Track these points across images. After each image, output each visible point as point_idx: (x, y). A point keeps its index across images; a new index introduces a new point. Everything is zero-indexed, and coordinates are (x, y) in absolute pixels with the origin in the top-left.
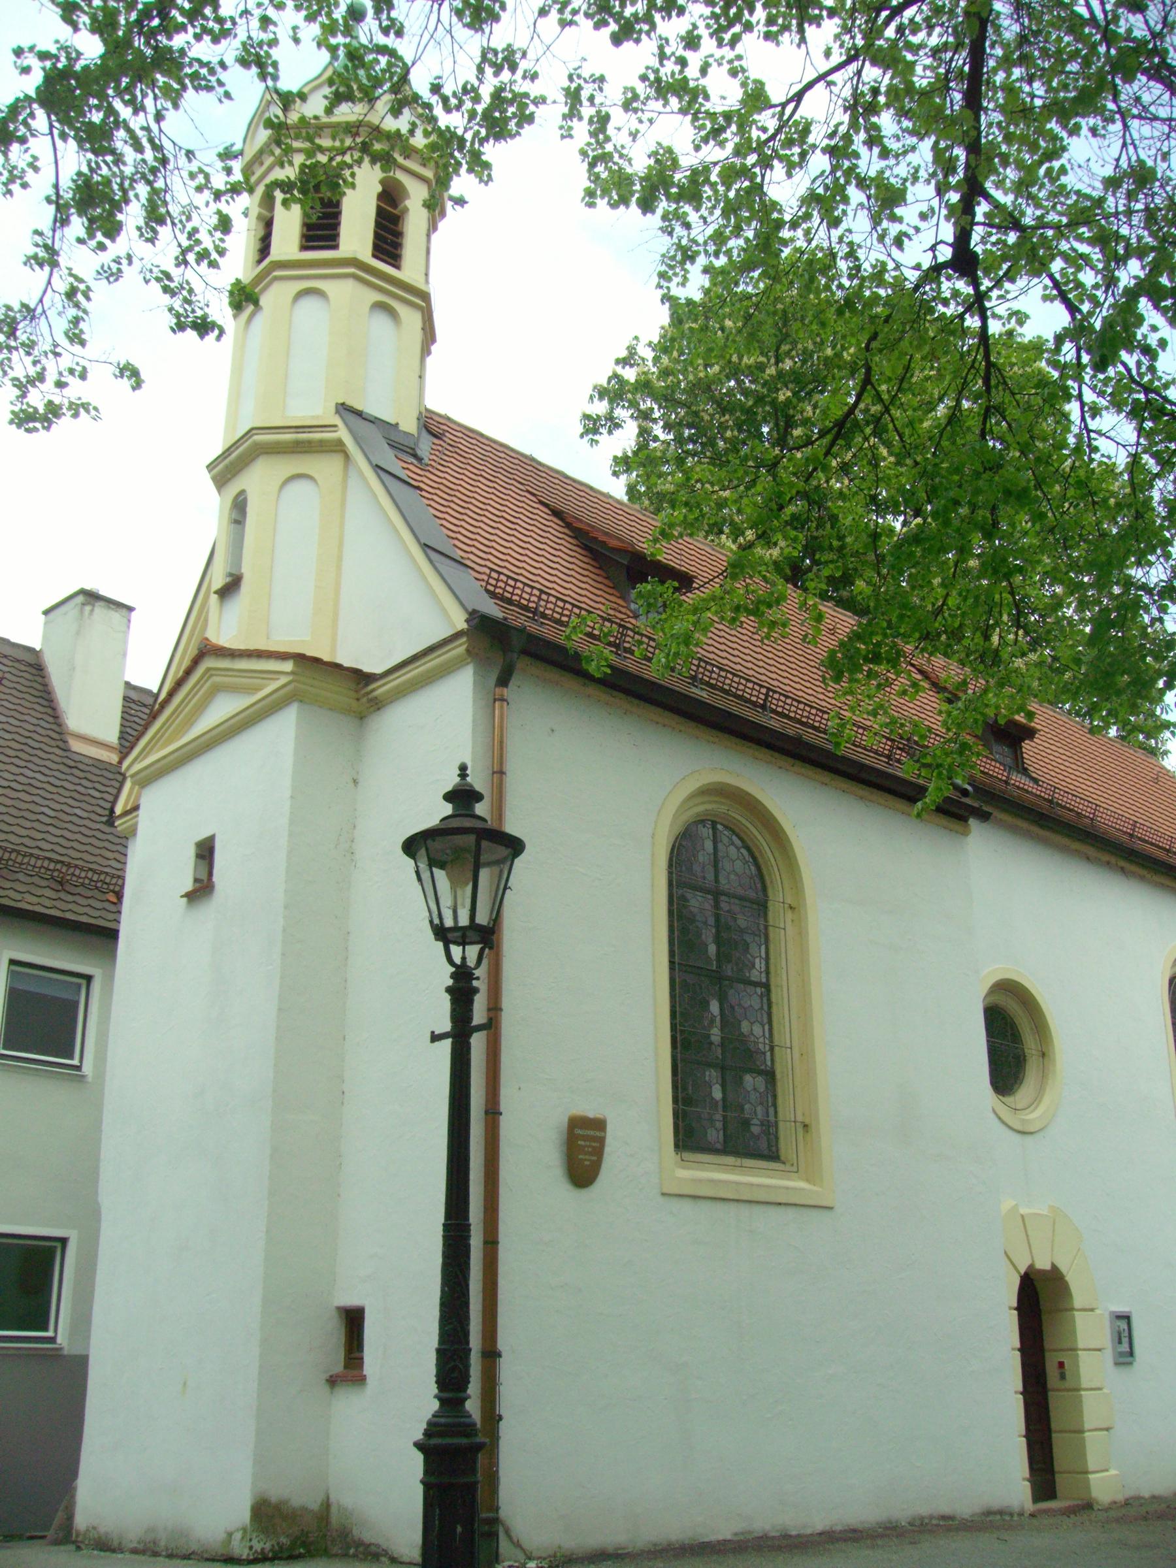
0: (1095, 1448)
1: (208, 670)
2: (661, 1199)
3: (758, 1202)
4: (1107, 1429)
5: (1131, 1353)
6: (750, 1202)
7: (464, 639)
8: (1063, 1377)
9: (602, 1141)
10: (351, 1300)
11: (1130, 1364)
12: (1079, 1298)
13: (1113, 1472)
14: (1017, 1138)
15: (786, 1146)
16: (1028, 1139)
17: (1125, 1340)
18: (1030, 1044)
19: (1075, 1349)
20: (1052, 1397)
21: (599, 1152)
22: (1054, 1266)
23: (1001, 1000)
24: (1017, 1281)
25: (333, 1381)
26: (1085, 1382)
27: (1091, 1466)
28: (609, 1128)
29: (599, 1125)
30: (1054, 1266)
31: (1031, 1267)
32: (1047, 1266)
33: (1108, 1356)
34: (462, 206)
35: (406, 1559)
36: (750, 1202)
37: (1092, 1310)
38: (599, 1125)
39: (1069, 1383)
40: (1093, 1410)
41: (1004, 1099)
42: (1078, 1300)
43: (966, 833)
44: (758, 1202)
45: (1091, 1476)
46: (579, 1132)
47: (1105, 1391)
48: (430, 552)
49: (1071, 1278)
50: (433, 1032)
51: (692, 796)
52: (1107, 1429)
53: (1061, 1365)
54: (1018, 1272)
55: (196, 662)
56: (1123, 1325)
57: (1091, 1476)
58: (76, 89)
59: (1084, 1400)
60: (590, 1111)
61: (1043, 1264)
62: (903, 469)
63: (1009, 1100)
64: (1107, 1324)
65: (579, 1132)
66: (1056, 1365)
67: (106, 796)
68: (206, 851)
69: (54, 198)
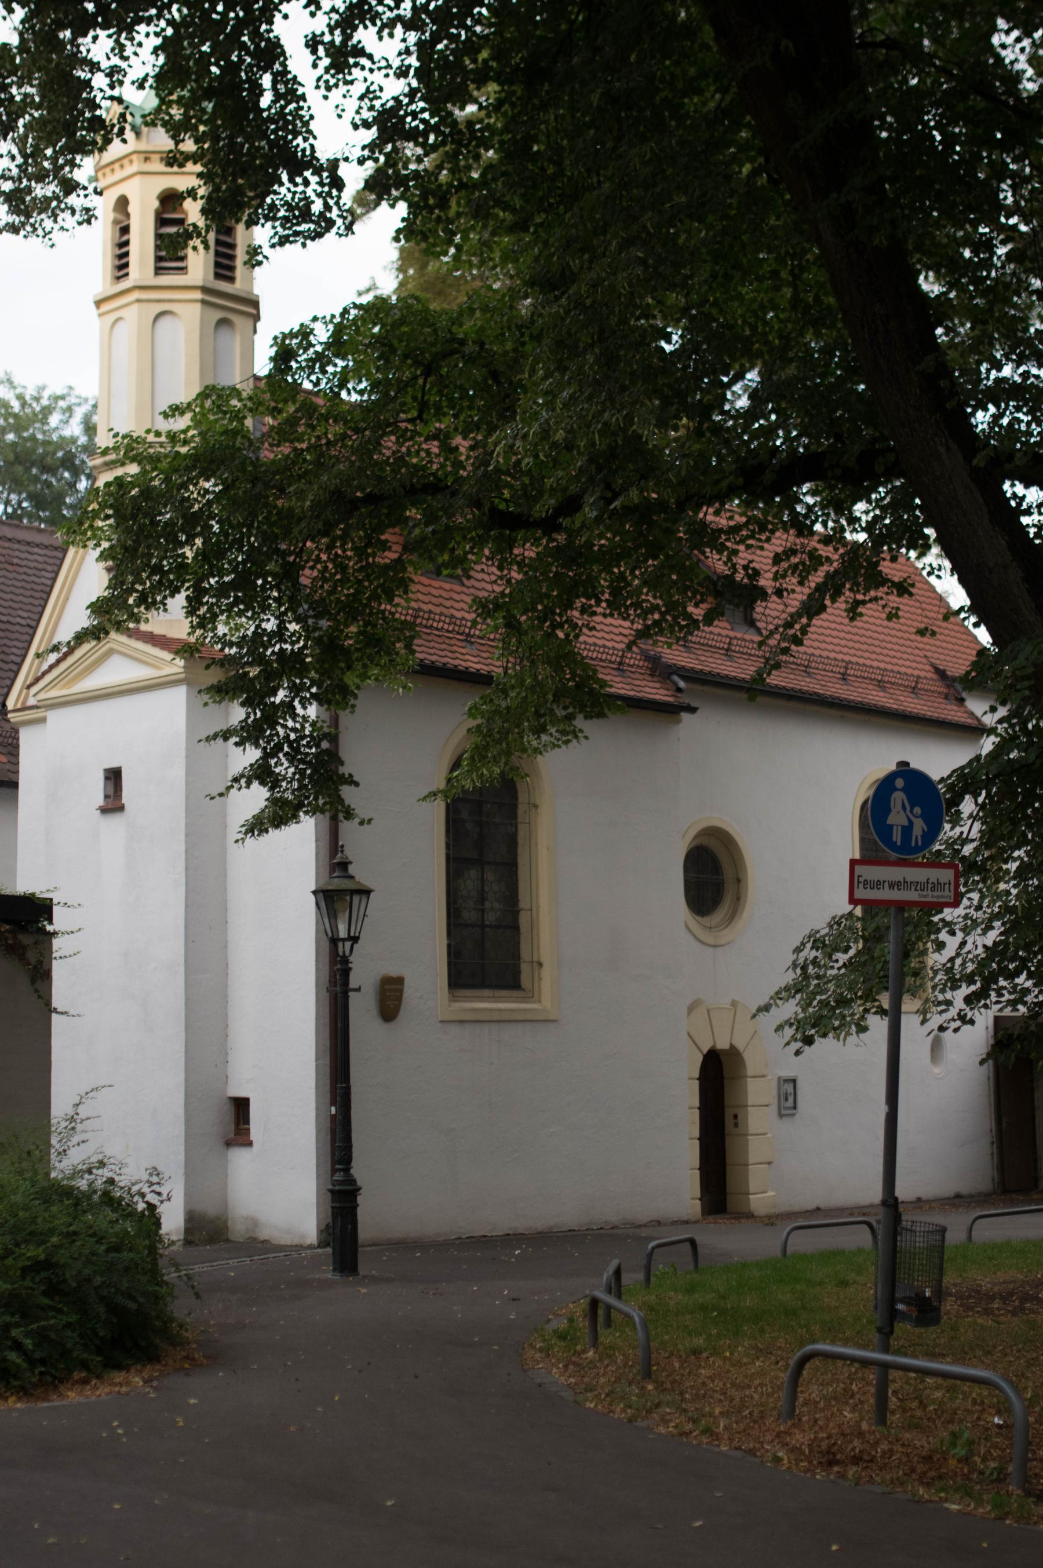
3: (504, 1021)
4: (769, 1163)
5: (795, 1108)
6: (498, 1021)
8: (736, 1125)
9: (401, 991)
11: (794, 1115)
13: (771, 1193)
14: (711, 949)
15: (525, 979)
17: (791, 1099)
18: (728, 874)
19: (747, 1106)
20: (728, 1140)
21: (399, 998)
22: (731, 1045)
23: (712, 844)
24: (699, 1059)
25: (229, 1144)
26: (752, 1129)
27: (752, 1189)
28: (406, 981)
29: (400, 981)
30: (731, 1045)
31: (714, 1046)
32: (727, 1046)
33: (773, 1109)
36: (498, 1021)
37: (763, 1076)
38: (400, 981)
40: (756, 1150)
41: (699, 918)
42: (751, 1070)
43: (679, 721)
44: (504, 1021)
45: (751, 1197)
46: (387, 987)
47: (769, 1135)
49: (748, 1057)
50: (104, 810)
52: (769, 1163)
53: (736, 1117)
54: (701, 1051)
56: (789, 1088)
57: (751, 1197)
59: (750, 1142)
60: (393, 972)
61: (723, 1044)
63: (706, 921)
64: (775, 1084)
65: (387, 987)
66: (732, 1117)
68: (114, 776)
69: (341, 816)
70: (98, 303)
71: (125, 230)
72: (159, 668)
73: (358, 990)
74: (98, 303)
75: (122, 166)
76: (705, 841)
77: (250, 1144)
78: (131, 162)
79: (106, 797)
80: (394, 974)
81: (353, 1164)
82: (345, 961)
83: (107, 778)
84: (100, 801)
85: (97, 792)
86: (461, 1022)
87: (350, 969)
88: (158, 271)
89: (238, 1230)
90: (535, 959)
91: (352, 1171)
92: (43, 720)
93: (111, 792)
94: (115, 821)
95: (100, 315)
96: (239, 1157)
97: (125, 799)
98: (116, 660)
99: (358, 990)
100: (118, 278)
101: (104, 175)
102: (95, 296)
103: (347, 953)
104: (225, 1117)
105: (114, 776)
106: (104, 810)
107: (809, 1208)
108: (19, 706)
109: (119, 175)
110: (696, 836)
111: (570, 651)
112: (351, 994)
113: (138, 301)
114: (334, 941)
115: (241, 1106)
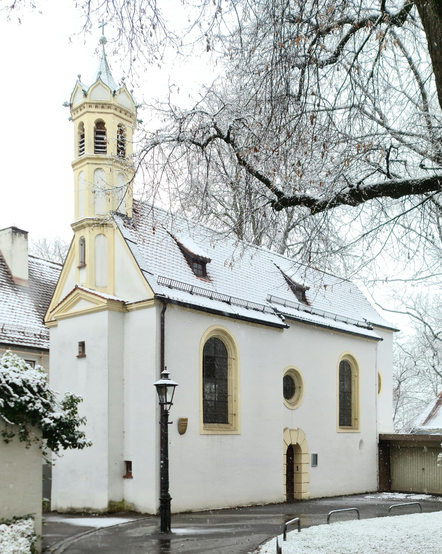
0: (304, 487)
1: (78, 293)
2: (200, 436)
7: (153, 301)
8: (298, 470)
9: (187, 424)
10: (129, 460)
12: (303, 450)
14: (291, 411)
16: (294, 411)
18: (297, 385)
22: (297, 443)
23: (293, 375)
24: (286, 448)
29: (186, 420)
30: (297, 443)
34: (308, 290)
35: (143, 510)
38: (186, 420)
39: (299, 471)
40: (304, 478)
41: (287, 400)
48: (128, 241)
49: (302, 447)
51: (212, 331)
53: (297, 467)
55: (74, 290)
58: (55, 436)
61: (294, 443)
62: (405, 296)
63: (289, 401)
67: (51, 292)
68: (82, 345)
70: (73, 166)
71: (83, 136)
72: (98, 304)
73: (172, 423)
74: (73, 166)
75: (81, 110)
76: (289, 374)
77: (132, 477)
78: (84, 107)
79: (80, 352)
80: (184, 418)
81: (169, 489)
82: (166, 412)
83: (80, 345)
84: (77, 354)
85: (76, 351)
86: (207, 435)
87: (169, 415)
88: (96, 152)
89: (125, 508)
90: (233, 413)
91: (169, 492)
92: (56, 326)
93: (81, 351)
94: (82, 362)
95: (74, 170)
96: (127, 482)
97: (87, 352)
98: (82, 302)
99: (172, 423)
100: (81, 152)
101: (74, 114)
102: (72, 162)
103: (168, 409)
104: (121, 469)
105: (82, 345)
106: (78, 357)
107: (320, 497)
108: (49, 320)
109: (80, 113)
110: (287, 372)
111: (397, 185)
112: (169, 425)
113: (88, 164)
114: (162, 404)
115: (129, 464)
